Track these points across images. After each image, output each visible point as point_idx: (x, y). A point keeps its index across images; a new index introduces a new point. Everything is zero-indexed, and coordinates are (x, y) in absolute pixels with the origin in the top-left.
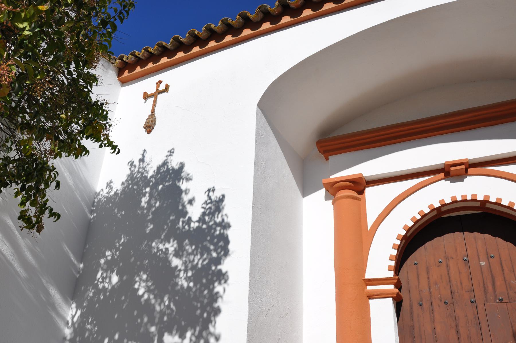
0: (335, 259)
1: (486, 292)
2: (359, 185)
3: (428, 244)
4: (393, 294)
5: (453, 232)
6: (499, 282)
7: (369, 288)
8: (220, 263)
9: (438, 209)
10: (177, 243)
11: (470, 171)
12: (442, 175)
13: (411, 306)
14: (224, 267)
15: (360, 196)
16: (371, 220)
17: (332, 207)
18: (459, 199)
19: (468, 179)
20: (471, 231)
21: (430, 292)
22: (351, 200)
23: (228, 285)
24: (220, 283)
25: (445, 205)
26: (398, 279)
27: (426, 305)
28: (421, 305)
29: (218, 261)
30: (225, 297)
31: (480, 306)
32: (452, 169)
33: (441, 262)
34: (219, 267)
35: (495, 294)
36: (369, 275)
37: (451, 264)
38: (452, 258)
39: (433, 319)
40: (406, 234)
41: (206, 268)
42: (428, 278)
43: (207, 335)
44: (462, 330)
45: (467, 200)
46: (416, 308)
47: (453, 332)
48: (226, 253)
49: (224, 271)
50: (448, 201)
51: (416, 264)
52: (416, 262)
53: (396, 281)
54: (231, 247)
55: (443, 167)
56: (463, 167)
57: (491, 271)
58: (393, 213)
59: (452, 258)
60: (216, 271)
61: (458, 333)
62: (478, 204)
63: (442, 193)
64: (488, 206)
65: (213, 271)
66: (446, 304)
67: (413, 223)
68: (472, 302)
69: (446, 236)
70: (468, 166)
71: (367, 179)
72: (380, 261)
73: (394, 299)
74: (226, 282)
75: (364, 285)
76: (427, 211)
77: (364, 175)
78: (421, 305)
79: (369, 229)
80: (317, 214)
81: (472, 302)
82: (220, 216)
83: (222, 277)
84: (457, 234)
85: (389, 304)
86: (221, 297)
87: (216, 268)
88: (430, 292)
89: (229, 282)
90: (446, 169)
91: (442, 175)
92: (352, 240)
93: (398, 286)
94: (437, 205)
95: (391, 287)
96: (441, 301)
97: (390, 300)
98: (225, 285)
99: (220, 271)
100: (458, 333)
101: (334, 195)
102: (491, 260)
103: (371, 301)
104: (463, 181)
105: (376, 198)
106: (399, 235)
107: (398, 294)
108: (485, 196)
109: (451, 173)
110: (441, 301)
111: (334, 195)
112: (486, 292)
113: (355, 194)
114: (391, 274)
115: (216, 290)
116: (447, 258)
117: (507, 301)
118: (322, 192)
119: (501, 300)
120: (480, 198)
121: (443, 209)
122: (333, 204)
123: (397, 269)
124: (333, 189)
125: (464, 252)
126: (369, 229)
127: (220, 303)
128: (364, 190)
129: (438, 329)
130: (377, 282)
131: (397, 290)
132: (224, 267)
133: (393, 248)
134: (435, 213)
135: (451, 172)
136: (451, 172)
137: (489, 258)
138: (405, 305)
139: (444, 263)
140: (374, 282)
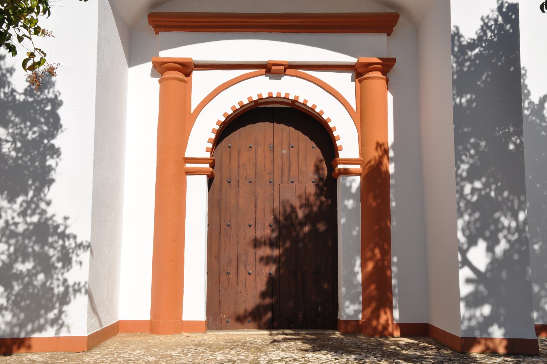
0: (158, 137)
1: (282, 175)
2: (186, 68)
3: (242, 129)
4: (209, 172)
5: (265, 122)
6: (294, 168)
7: (188, 165)
8: (53, 136)
9: (256, 101)
10: (152, 363)
11: (288, 71)
12: (264, 71)
13: (221, 183)
14: (57, 142)
15: (186, 79)
16: (195, 104)
17: (158, 85)
18: (275, 95)
19: (285, 78)
20: (279, 123)
21: (239, 172)
22: (178, 81)
23: (60, 160)
24: (52, 157)
25: (262, 99)
26: (214, 160)
27: (233, 183)
28: (229, 182)
29: (52, 135)
30: (57, 169)
31: (277, 186)
32: (273, 68)
33: (251, 147)
34: (53, 142)
35: (289, 177)
36: (188, 155)
37: (260, 149)
38: (260, 144)
39: (238, 195)
40: (225, 120)
41: (37, 143)
42: (239, 160)
43: (38, 200)
44: (259, 204)
45: (280, 98)
46: (225, 185)
47: (253, 205)
48: (55, 125)
49: (57, 146)
50: (265, 96)
51: (229, 147)
52: (230, 145)
53: (211, 161)
54: (62, 122)
55: (266, 63)
56: (283, 68)
57: (289, 159)
58: (216, 98)
59: (260, 144)
60: (49, 144)
61: (256, 206)
62: (290, 102)
63: (261, 87)
64: (297, 104)
65: (45, 145)
66: (250, 182)
67: (232, 112)
68: (270, 182)
69: (257, 124)
70: (287, 66)
71: (195, 63)
72: (199, 142)
73: (208, 176)
74: (58, 157)
75: (184, 162)
76: (246, 102)
77: (194, 59)
78: (229, 182)
79: (192, 112)
80: (142, 87)
81: (270, 182)
82: (51, 91)
83: (55, 152)
84: (267, 123)
85: (204, 179)
86: (54, 169)
87: (49, 141)
88: (239, 172)
89: (61, 157)
90: (268, 66)
91: (264, 71)
92: (175, 119)
93: (212, 165)
94: (255, 98)
95: (207, 166)
96: (246, 180)
97: (206, 176)
98: (58, 160)
99: (53, 146)
100: (256, 206)
101: (162, 73)
102: (291, 149)
103: (189, 177)
104: (280, 79)
105: (202, 83)
106: (219, 121)
107: (212, 172)
108: (338, 136)
109: (272, 71)
110: (246, 180)
111: (162, 73)
112: (282, 175)
113: (181, 76)
114: (208, 155)
115: (48, 163)
116: (256, 144)
117: (297, 183)
118: (148, 66)
119: (292, 182)
120: (292, 97)
121: (260, 101)
122: (160, 82)
123: (212, 150)
124: (161, 68)
125: (271, 141)
126: (192, 112)
127: (53, 175)
128: (191, 73)
129: (241, 203)
130: (195, 161)
131: (211, 169)
132: (57, 142)
133: (212, 132)
134: (253, 104)
135: (271, 69)
136: (271, 69)
137: (290, 147)
138: (216, 181)
139: (253, 149)
140: (192, 161)
